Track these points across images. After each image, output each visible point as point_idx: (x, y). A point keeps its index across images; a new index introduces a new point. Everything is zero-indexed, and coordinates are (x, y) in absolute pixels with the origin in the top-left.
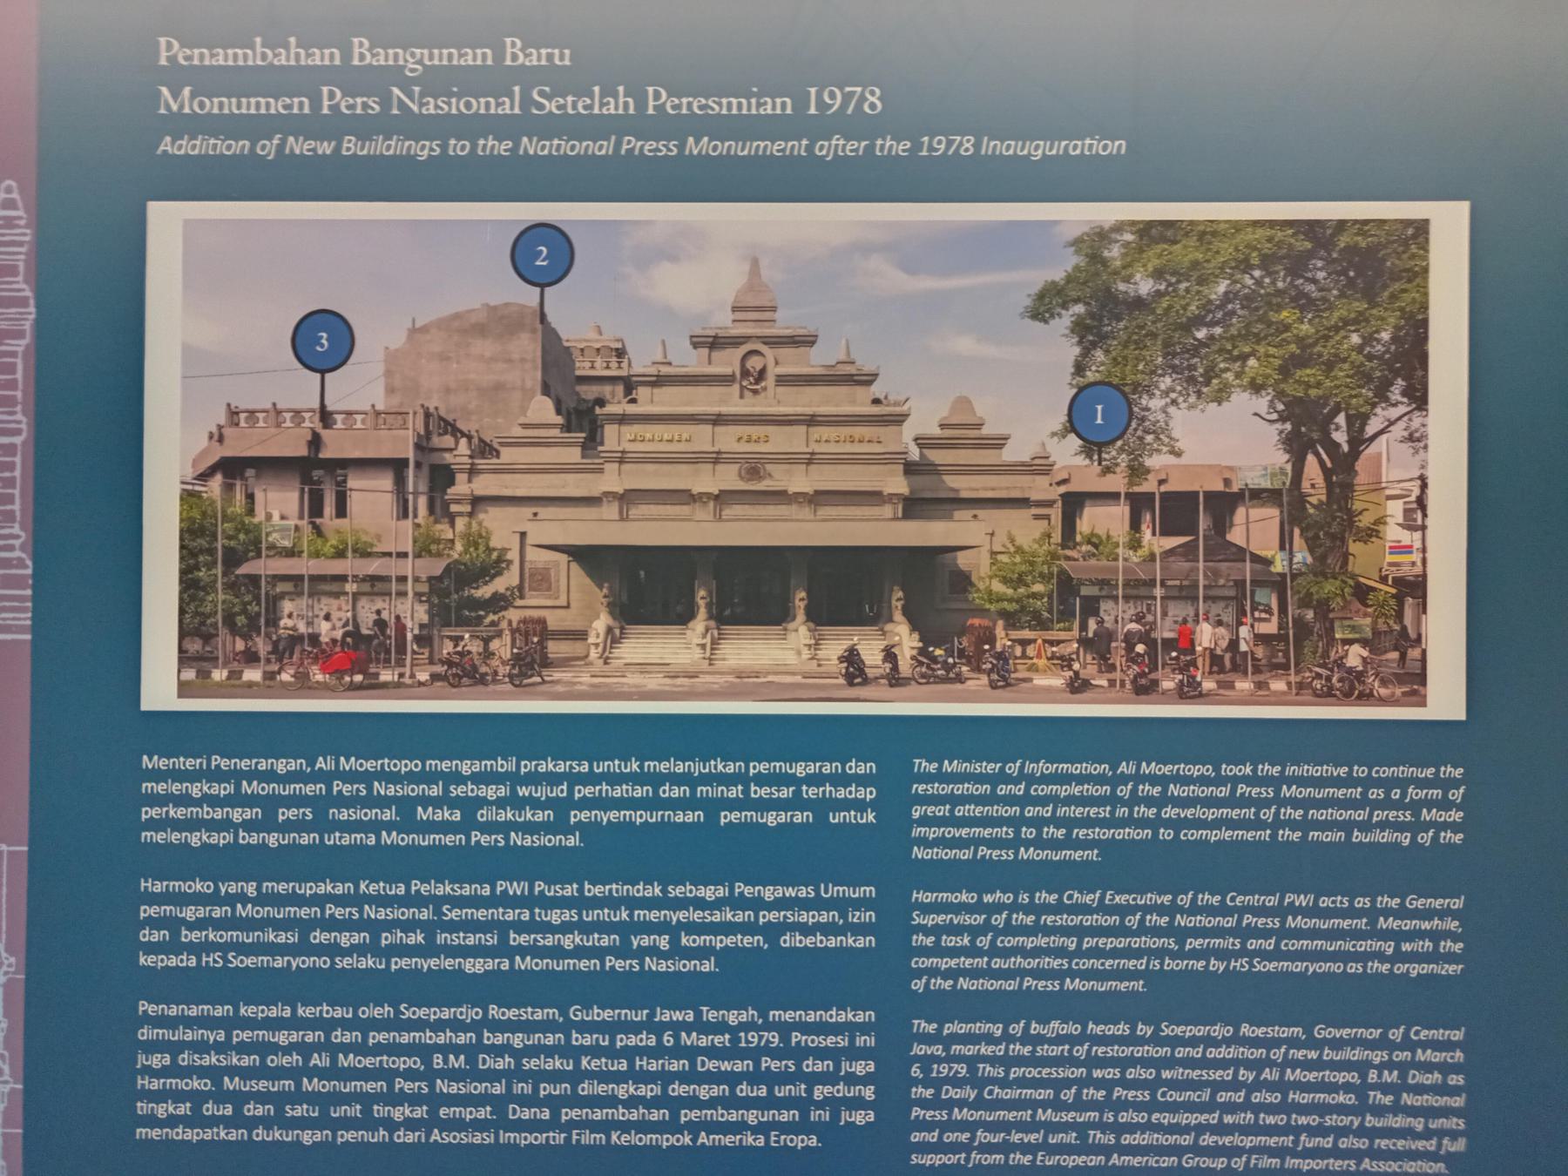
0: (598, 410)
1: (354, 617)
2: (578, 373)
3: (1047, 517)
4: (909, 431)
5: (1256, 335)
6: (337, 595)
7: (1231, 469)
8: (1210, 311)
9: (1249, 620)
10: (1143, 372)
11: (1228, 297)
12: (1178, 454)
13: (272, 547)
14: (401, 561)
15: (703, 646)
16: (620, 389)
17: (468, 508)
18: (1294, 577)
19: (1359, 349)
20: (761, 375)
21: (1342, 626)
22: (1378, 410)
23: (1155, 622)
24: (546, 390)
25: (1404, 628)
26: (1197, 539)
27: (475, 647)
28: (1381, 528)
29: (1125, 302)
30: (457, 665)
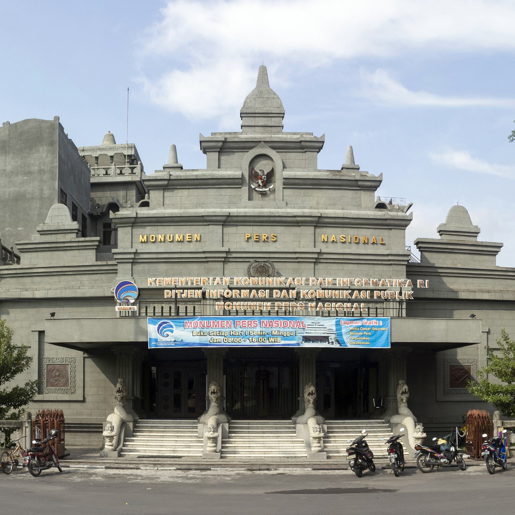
0: (112, 215)
2: (93, 180)
4: (412, 234)
15: (215, 440)
16: (133, 193)
24: (63, 198)
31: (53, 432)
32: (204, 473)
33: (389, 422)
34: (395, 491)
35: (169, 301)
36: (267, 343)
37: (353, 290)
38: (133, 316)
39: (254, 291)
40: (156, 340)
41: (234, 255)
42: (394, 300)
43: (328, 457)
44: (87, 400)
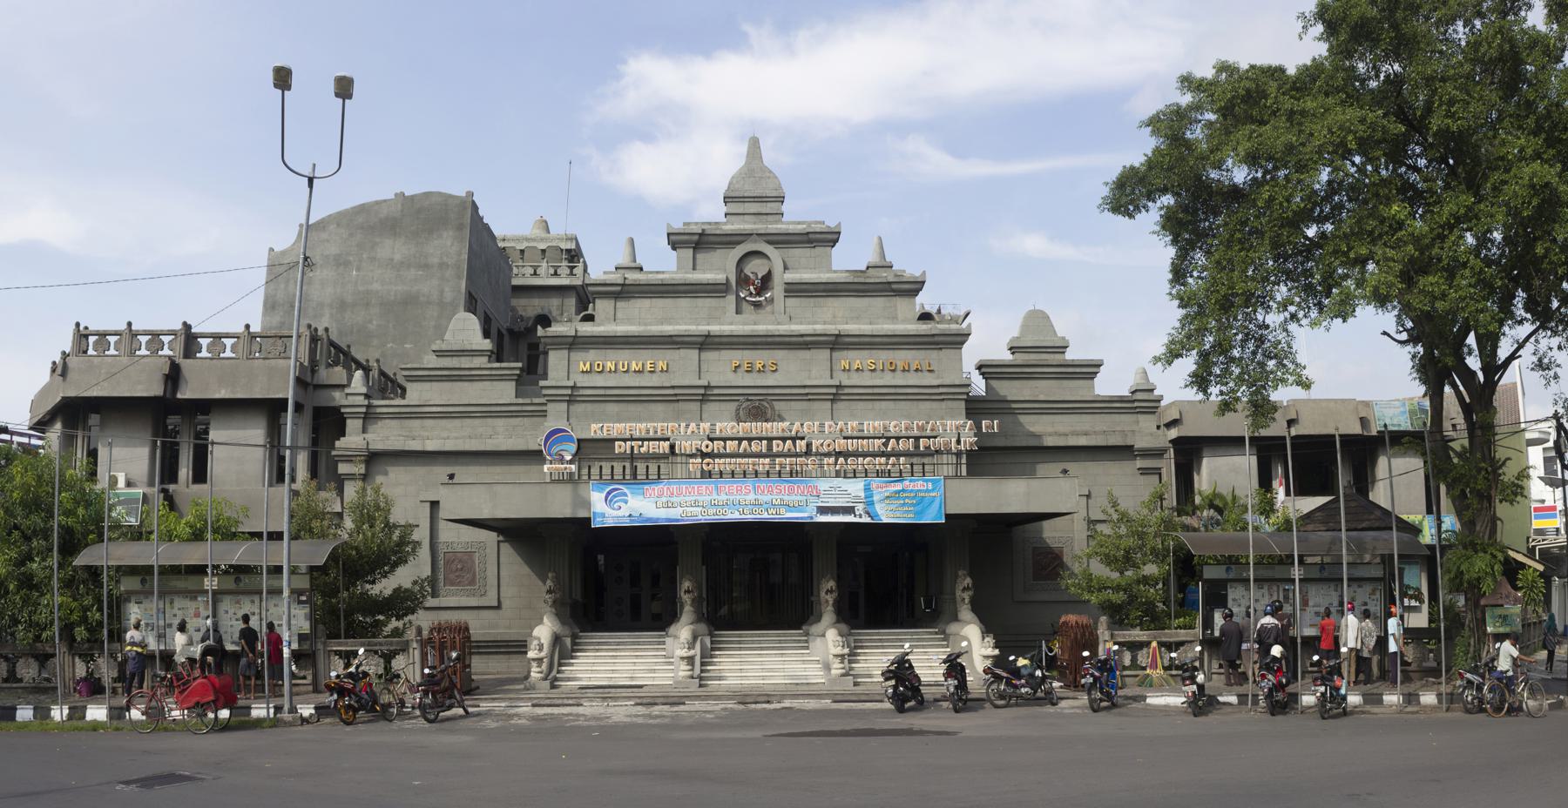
0: (540, 331)
1: (216, 631)
2: (515, 282)
3: (1157, 472)
4: (971, 355)
5: (1371, 233)
6: (193, 594)
7: (1367, 404)
8: (1315, 204)
9: (1396, 610)
10: (1253, 279)
11: (1333, 187)
12: (1306, 385)
13: (116, 526)
14: (274, 545)
15: (690, 660)
16: (571, 302)
17: (361, 469)
18: (1443, 549)
19: (1476, 251)
20: (766, 282)
21: (1493, 617)
22: (1506, 329)
23: (1294, 615)
24: (472, 305)
25: (1552, 617)
26: (1337, 500)
27: (373, 667)
28: (1524, 483)
29: (1220, 193)
30: (350, 692)
31: (454, 655)
32: (676, 708)
33: (944, 632)
34: (954, 733)
35: (621, 457)
36: (766, 515)
37: (888, 439)
38: (571, 479)
39: (745, 443)
40: (603, 515)
41: (716, 391)
42: (949, 452)
43: (856, 684)
44: (504, 605)
